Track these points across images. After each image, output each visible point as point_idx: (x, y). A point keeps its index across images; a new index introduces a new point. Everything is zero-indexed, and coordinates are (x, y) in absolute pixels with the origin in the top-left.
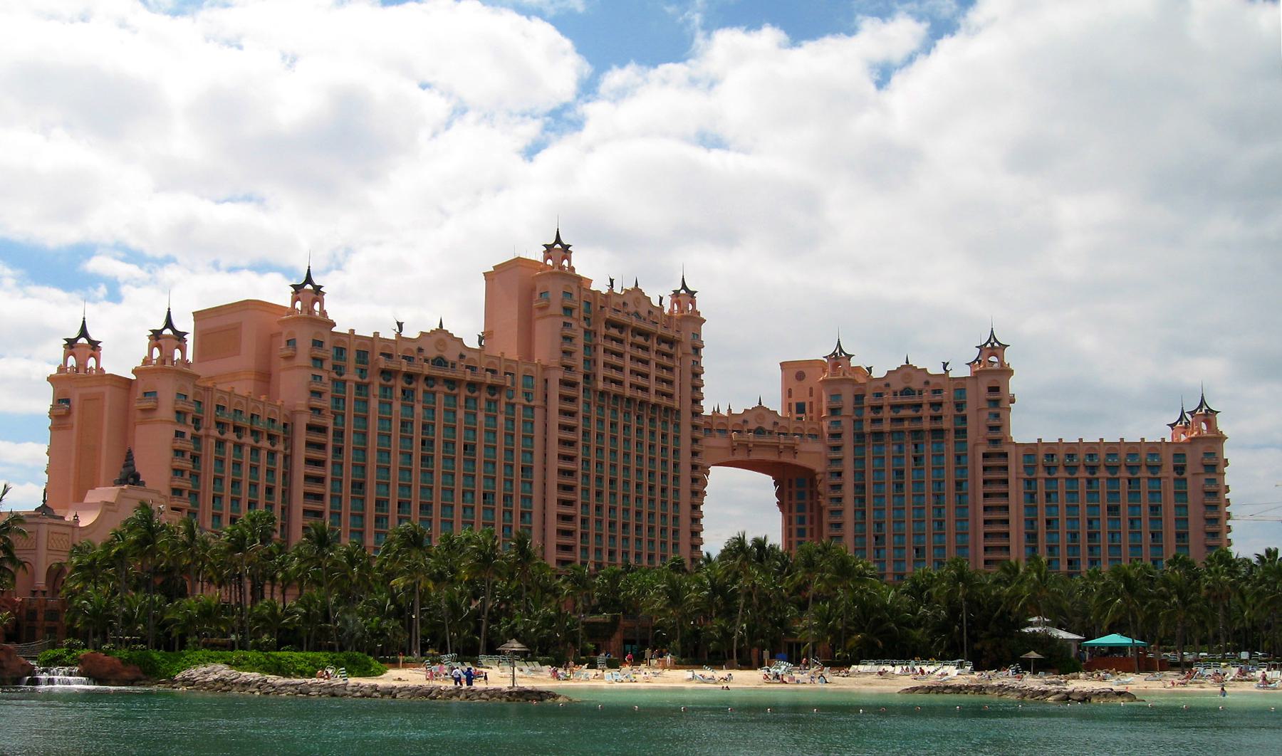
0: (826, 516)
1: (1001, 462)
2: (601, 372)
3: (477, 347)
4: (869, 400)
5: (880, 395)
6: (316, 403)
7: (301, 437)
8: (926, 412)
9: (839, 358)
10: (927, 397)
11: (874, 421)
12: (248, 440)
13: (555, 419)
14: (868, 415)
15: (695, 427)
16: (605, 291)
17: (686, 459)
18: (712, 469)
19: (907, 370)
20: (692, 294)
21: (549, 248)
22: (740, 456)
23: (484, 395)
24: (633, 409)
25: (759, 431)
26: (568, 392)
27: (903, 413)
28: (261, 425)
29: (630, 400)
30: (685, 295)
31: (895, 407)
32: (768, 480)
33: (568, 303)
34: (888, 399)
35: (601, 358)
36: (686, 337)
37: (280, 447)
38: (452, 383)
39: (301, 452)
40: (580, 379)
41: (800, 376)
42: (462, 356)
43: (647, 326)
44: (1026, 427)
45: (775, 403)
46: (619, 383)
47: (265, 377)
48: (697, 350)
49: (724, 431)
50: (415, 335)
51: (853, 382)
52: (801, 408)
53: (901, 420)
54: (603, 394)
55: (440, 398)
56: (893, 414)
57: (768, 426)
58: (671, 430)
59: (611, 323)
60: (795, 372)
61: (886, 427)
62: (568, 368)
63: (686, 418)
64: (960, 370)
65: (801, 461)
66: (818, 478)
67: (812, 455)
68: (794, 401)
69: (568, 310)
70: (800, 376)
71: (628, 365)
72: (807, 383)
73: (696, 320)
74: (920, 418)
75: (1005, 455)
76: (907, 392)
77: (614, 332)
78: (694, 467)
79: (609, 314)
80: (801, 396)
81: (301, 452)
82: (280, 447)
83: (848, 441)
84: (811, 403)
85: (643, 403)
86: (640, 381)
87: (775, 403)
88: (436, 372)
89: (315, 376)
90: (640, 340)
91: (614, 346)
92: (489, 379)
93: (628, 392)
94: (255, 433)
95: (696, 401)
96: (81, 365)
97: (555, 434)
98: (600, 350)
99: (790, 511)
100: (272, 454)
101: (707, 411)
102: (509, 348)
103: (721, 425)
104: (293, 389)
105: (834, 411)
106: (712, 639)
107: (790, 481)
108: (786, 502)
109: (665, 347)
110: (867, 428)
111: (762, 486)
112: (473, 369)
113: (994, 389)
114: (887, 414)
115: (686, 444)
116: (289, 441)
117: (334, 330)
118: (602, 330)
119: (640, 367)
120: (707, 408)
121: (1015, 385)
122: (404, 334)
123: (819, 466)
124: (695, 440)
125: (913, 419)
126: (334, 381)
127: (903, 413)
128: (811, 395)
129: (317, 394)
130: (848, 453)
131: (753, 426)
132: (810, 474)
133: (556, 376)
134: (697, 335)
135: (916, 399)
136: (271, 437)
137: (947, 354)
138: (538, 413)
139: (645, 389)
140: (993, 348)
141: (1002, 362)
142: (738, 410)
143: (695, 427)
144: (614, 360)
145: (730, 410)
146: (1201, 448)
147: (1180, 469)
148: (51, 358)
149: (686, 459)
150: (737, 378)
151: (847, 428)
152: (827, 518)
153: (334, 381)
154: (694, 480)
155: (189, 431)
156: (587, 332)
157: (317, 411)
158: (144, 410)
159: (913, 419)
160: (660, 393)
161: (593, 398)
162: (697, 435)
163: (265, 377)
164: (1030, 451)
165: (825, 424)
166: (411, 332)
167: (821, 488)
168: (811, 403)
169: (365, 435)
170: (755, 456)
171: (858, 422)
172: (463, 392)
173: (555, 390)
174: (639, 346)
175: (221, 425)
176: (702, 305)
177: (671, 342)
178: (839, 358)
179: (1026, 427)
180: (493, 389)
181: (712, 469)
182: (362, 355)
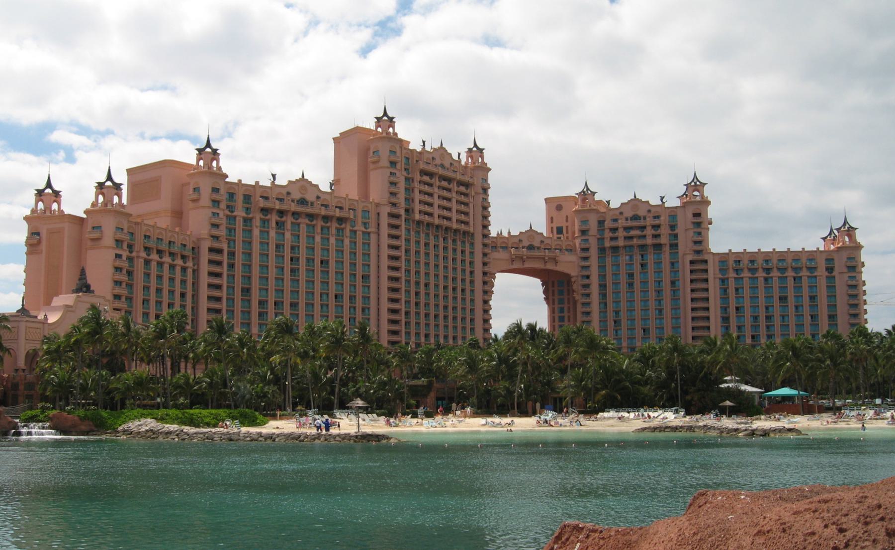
2: (417, 207)
3: (329, 190)
4: (608, 224)
5: (616, 220)
6: (215, 232)
7: (205, 256)
8: (649, 232)
9: (586, 194)
10: (649, 221)
11: (612, 239)
13: (385, 241)
14: (608, 234)
15: (485, 245)
16: (419, 149)
17: (478, 269)
21: (379, 119)
22: (517, 265)
24: (441, 233)
28: (176, 249)
30: (476, 152)
31: (626, 229)
32: (537, 282)
33: (393, 158)
34: (622, 223)
35: (417, 197)
37: (190, 264)
38: (311, 216)
41: (559, 208)
43: (431, 168)
44: (720, 242)
45: (541, 227)
47: (178, 215)
48: (485, 190)
52: (560, 230)
53: (631, 238)
54: (419, 223)
56: (625, 234)
57: (536, 244)
59: (423, 173)
60: (555, 205)
61: (621, 243)
62: (394, 205)
64: (673, 202)
65: (559, 268)
66: (573, 280)
67: (568, 264)
68: (555, 225)
69: (393, 164)
70: (559, 208)
72: (563, 213)
73: (485, 169)
74: (644, 236)
75: (706, 262)
76: (635, 218)
77: (426, 178)
78: (485, 274)
79: (422, 166)
80: (560, 222)
81: (205, 268)
82: (190, 264)
83: (594, 253)
84: (567, 227)
85: (447, 229)
87: (541, 227)
89: (214, 214)
90: (445, 184)
92: (338, 213)
95: (485, 227)
96: (48, 208)
98: (417, 191)
99: (553, 304)
100: (184, 269)
102: (351, 191)
103: (503, 243)
104: (198, 223)
105: (583, 232)
107: (553, 282)
108: (551, 298)
109: (462, 189)
110: (607, 244)
111: (533, 286)
113: (697, 215)
114: (621, 233)
115: (478, 259)
117: (227, 180)
118: (418, 177)
119: (445, 203)
122: (277, 182)
123: (573, 272)
124: (485, 255)
126: (227, 216)
128: (567, 221)
130: (594, 262)
131: (526, 243)
132: (568, 277)
133: (386, 210)
134: (485, 180)
136: (183, 257)
138: (373, 237)
140: (696, 185)
141: (702, 196)
143: (485, 245)
145: (509, 233)
146: (845, 255)
147: (830, 270)
148: (26, 204)
149: (478, 269)
150: (514, 212)
152: (579, 309)
153: (227, 216)
154: (485, 283)
155: (125, 254)
156: (407, 179)
157: (216, 238)
158: (92, 240)
159: (640, 237)
161: (412, 226)
163: (178, 215)
164: (723, 259)
166: (281, 181)
167: (575, 287)
168: (567, 227)
170: (528, 265)
171: (601, 240)
173: (385, 221)
174: (444, 189)
175: (147, 249)
176: (489, 159)
177: (467, 185)
179: (720, 242)
180: (341, 220)
181: (498, 275)
182: (247, 198)
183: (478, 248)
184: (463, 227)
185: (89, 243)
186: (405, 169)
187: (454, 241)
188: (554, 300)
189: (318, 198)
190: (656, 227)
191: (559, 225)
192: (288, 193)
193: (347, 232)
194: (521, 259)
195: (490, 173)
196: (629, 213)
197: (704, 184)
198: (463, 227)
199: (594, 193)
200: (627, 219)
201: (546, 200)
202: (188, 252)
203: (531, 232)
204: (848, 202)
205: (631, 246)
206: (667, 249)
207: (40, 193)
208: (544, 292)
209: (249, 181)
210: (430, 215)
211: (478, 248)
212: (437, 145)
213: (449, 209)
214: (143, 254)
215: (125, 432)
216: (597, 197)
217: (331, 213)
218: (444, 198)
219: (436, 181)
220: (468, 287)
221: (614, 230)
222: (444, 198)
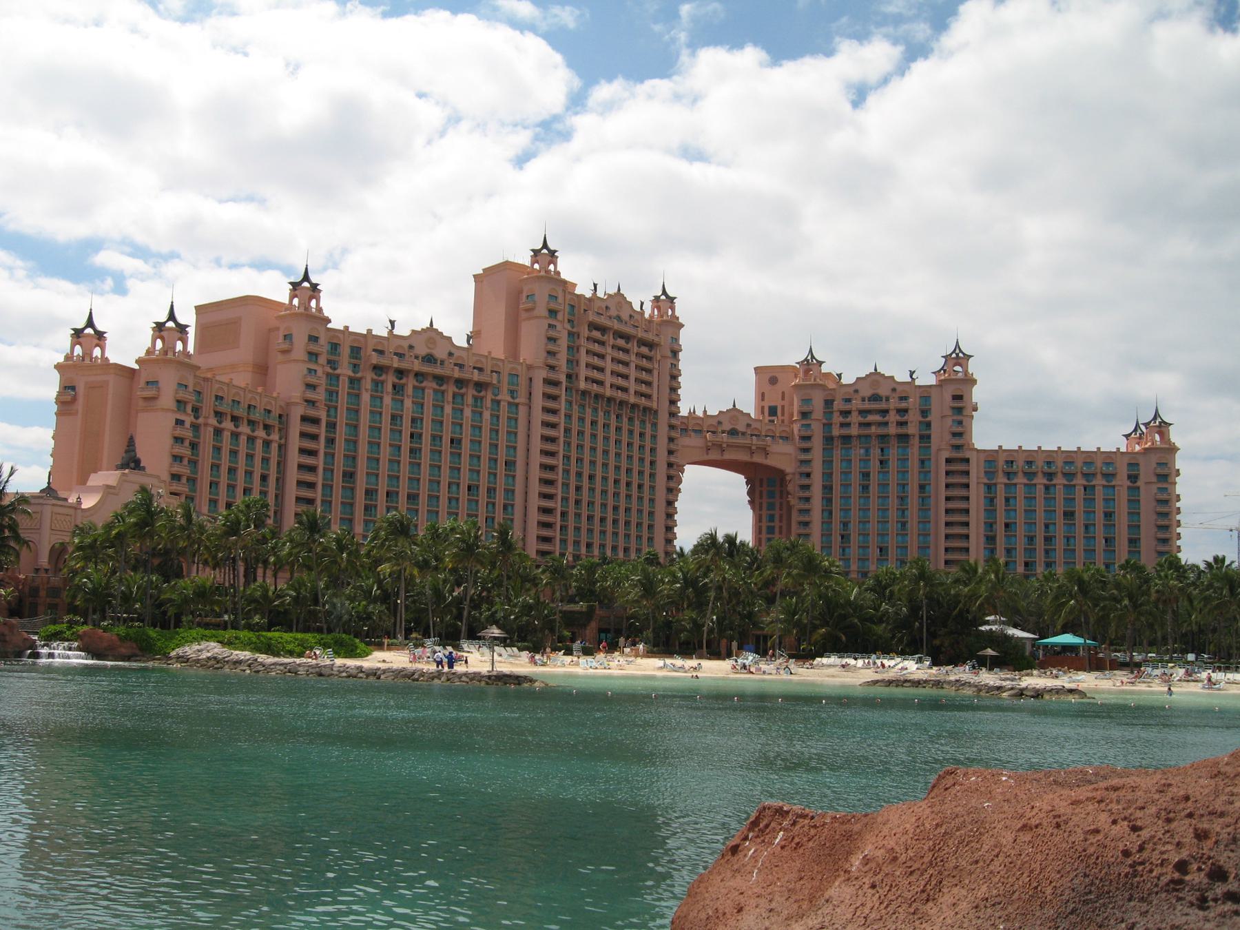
2: (583, 372)
3: (466, 345)
4: (838, 405)
5: (848, 400)
6: (311, 395)
7: (295, 427)
8: (893, 417)
9: (810, 364)
10: (894, 404)
11: (842, 425)
12: (244, 429)
14: (837, 419)
15: (672, 427)
16: (588, 294)
18: (687, 467)
20: (671, 300)
27: (870, 418)
28: (257, 416)
29: (634, 406)
30: (665, 301)
31: (863, 412)
33: (553, 306)
34: (856, 404)
35: (584, 358)
36: (665, 341)
37: (275, 437)
38: (440, 379)
39: (295, 442)
40: (563, 378)
42: (451, 354)
43: (602, 321)
44: (987, 435)
45: (749, 406)
47: (262, 370)
48: (675, 353)
50: (406, 333)
52: (773, 411)
53: (868, 425)
54: (584, 393)
55: (429, 394)
56: (861, 419)
57: (741, 427)
58: (648, 431)
59: (593, 326)
60: (768, 377)
61: (854, 431)
62: (552, 368)
63: (663, 419)
64: (926, 379)
66: (788, 478)
67: (783, 457)
68: (767, 404)
70: (773, 381)
72: (779, 387)
73: (676, 325)
74: (886, 424)
76: (875, 398)
78: (670, 465)
79: (592, 317)
80: (774, 399)
81: (295, 442)
82: (275, 437)
83: (817, 444)
84: (783, 407)
87: (749, 406)
88: (426, 369)
89: (310, 370)
90: (621, 342)
92: (476, 376)
94: (251, 423)
95: (673, 402)
96: (87, 354)
97: (538, 431)
98: (583, 351)
99: (761, 509)
100: (267, 444)
101: (684, 412)
102: (496, 347)
103: (695, 425)
104: (289, 382)
105: (804, 415)
107: (761, 480)
108: (757, 501)
109: (644, 350)
110: (836, 432)
111: (735, 484)
112: (461, 366)
114: (855, 418)
117: (329, 326)
118: (585, 332)
120: (684, 409)
121: (978, 394)
122: (396, 332)
123: (789, 467)
124: (671, 440)
125: (880, 424)
126: (328, 374)
127: (870, 418)
128: (783, 398)
130: (817, 455)
134: (676, 339)
135: (883, 406)
136: (267, 427)
137: (915, 363)
138: (522, 411)
139: (625, 390)
140: (958, 358)
141: (966, 372)
142: (713, 412)
143: (672, 427)
144: (596, 361)
145: (705, 412)
146: (1154, 459)
147: (1133, 478)
150: (712, 383)
152: (795, 517)
153: (328, 374)
154: (670, 478)
155: (189, 420)
156: (570, 334)
157: (311, 403)
159: (880, 424)
161: (575, 397)
162: (673, 434)
163: (262, 370)
164: (991, 458)
165: (796, 427)
166: (402, 330)
167: (790, 488)
168: (783, 407)
170: (728, 456)
171: (828, 426)
177: (651, 345)
178: (810, 364)
179: (987, 435)
180: (480, 386)
181: (687, 467)
182: (356, 351)
183: (663, 430)
184: (643, 401)
186: (569, 321)
187: (631, 419)
188: (761, 504)
189: (451, 354)
191: (772, 404)
192: (411, 347)
194: (720, 447)
195: (682, 331)
198: (643, 401)
199: (820, 363)
200: (863, 400)
201: (756, 369)
202: (273, 421)
203: (734, 412)
205: (868, 436)
206: (915, 441)
208: (749, 493)
209: (359, 328)
211: (663, 430)
212: (613, 291)
219: (610, 339)
221: (846, 413)
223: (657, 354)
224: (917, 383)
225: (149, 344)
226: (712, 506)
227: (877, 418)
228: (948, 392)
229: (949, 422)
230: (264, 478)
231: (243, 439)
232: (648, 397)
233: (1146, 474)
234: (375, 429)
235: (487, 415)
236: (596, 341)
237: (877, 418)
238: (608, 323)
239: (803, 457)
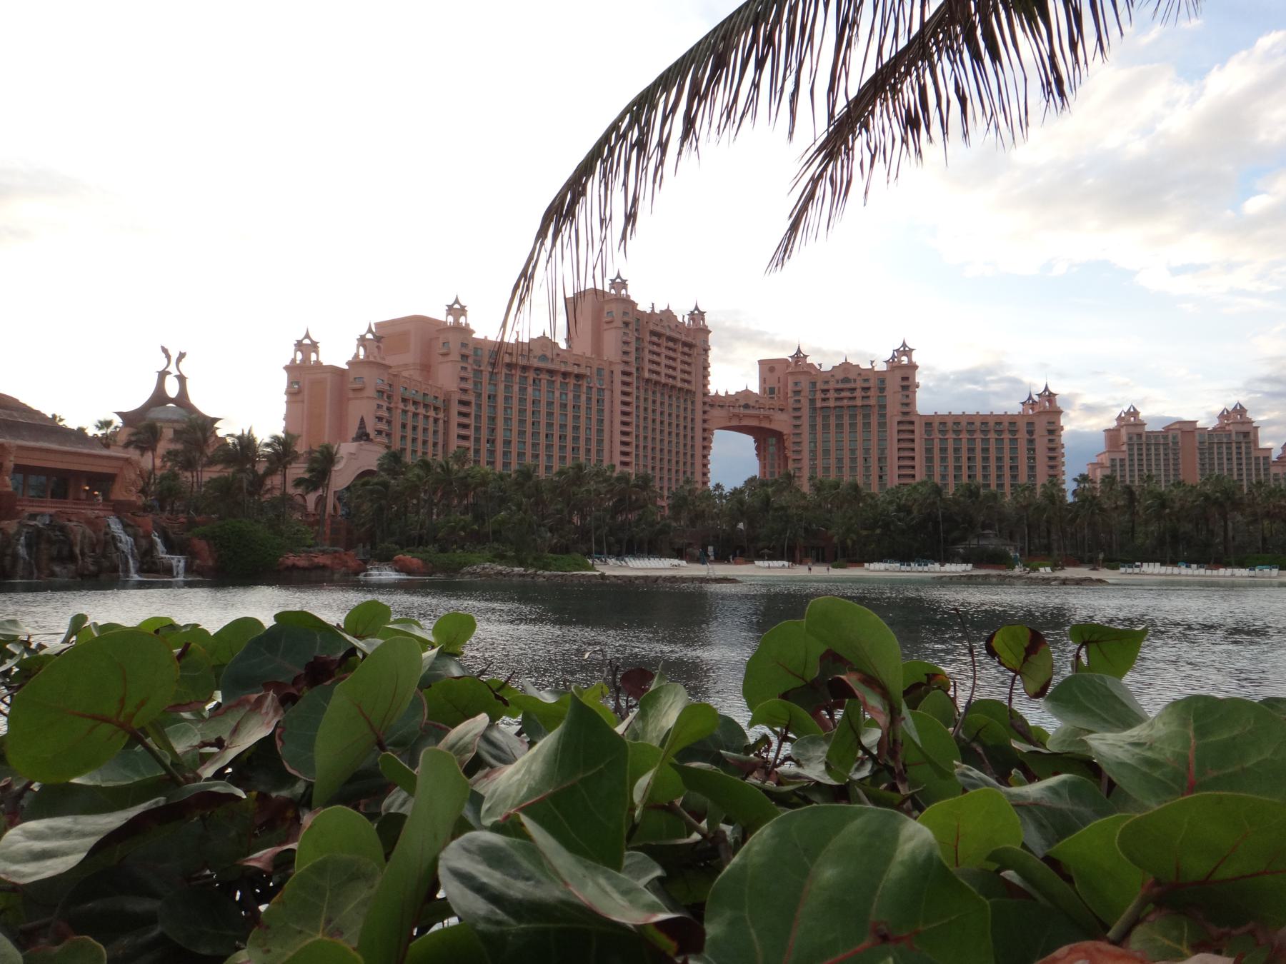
0: (790, 462)
1: (910, 428)
2: (647, 366)
4: (820, 386)
5: (827, 382)
6: (464, 385)
7: (455, 408)
8: (858, 393)
9: (799, 356)
10: (859, 384)
12: (421, 410)
13: (618, 398)
14: (819, 395)
15: (704, 403)
16: (649, 311)
17: (699, 426)
18: (716, 432)
19: (846, 366)
20: (702, 314)
22: (734, 423)
23: (559, 379)
24: (658, 388)
25: (747, 406)
26: (626, 379)
28: (430, 400)
29: (665, 385)
30: (697, 315)
31: (837, 390)
33: (626, 319)
34: (832, 385)
35: (648, 356)
36: (698, 342)
37: (441, 415)
39: (455, 419)
40: (634, 370)
43: (658, 329)
44: (927, 402)
45: (755, 388)
46: (658, 373)
47: (426, 368)
48: (706, 350)
49: (722, 406)
51: (808, 373)
52: (772, 391)
53: (842, 399)
54: (648, 381)
57: (752, 403)
58: (689, 406)
59: (653, 333)
60: (768, 367)
61: (832, 404)
62: (626, 363)
63: (699, 399)
64: (881, 367)
65: (773, 426)
67: (782, 422)
68: (767, 386)
69: (626, 324)
70: (772, 369)
71: (679, 366)
73: (706, 331)
75: (912, 423)
76: (846, 380)
77: (655, 339)
78: (704, 430)
79: (652, 327)
80: (773, 383)
81: (455, 419)
82: (441, 415)
83: (806, 412)
85: (657, 383)
86: (671, 372)
87: (755, 388)
90: (671, 344)
91: (655, 348)
92: (576, 370)
93: (663, 380)
94: (426, 406)
95: (705, 386)
96: (306, 358)
97: (619, 408)
98: (646, 351)
100: (436, 420)
101: (713, 392)
102: (584, 347)
104: (447, 378)
105: (797, 393)
106: (425, 644)
109: (686, 349)
110: (819, 404)
111: (746, 443)
113: (905, 379)
114: (832, 395)
115: (699, 416)
116: (447, 410)
118: (648, 338)
119: (671, 363)
120: (712, 389)
121: (920, 378)
124: (705, 412)
126: (475, 370)
129: (463, 379)
130: (805, 422)
131: (742, 403)
133: (618, 369)
134: (706, 341)
135: (852, 385)
136: (436, 409)
137: (873, 352)
139: (674, 378)
140: (905, 351)
141: (910, 360)
142: (732, 392)
143: (704, 403)
144: (655, 358)
146: (1045, 419)
147: (1031, 433)
148: (288, 354)
149: (699, 426)
150: (731, 374)
151: (805, 403)
153: (475, 370)
154: (704, 439)
155: (385, 405)
156: (638, 339)
157: (465, 391)
158: (355, 390)
160: (684, 381)
161: (642, 384)
162: (707, 408)
163: (426, 368)
164: (929, 422)
165: (791, 401)
169: (495, 407)
170: (745, 422)
171: (812, 401)
172: (572, 381)
173: (618, 378)
174: (654, 344)
175: (404, 400)
176: (709, 320)
177: (690, 346)
178: (799, 356)
179: (927, 402)
180: (578, 377)
181: (716, 432)
183: (699, 407)
184: (686, 386)
185: (351, 395)
187: (654, 393)
190: (866, 389)
193: (584, 389)
194: (736, 416)
195: (710, 335)
196: (840, 376)
197: (911, 350)
198: (686, 386)
199: (806, 356)
202: (439, 403)
203: (747, 393)
204: (1243, 399)
207: (299, 345)
210: (658, 373)
211: (699, 407)
212: (664, 308)
213: (658, 364)
214: (401, 405)
215: (469, 573)
216: (809, 360)
217: (569, 369)
218: (654, 353)
219: (663, 342)
220: (689, 442)
221: (825, 391)
222: (654, 353)
223: (695, 352)
224: (876, 369)
225: (355, 351)
226: (732, 461)
227: (848, 394)
228: (899, 374)
229: (899, 396)
230: (435, 444)
231: (431, 420)
232: (689, 382)
233: (1040, 430)
234: (522, 411)
235: (516, 388)
236: (654, 344)
237: (848, 394)
238: (663, 331)
239: (1051, 472)
